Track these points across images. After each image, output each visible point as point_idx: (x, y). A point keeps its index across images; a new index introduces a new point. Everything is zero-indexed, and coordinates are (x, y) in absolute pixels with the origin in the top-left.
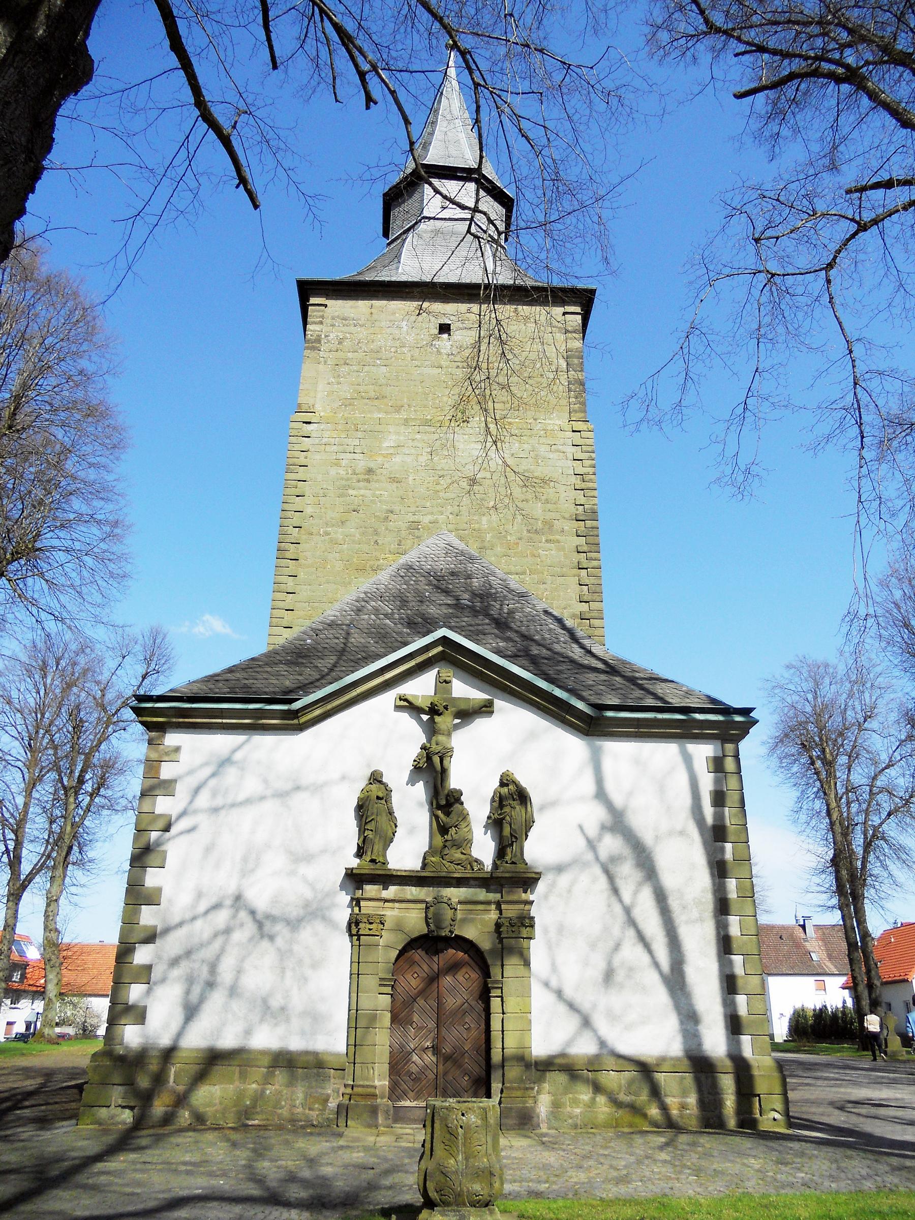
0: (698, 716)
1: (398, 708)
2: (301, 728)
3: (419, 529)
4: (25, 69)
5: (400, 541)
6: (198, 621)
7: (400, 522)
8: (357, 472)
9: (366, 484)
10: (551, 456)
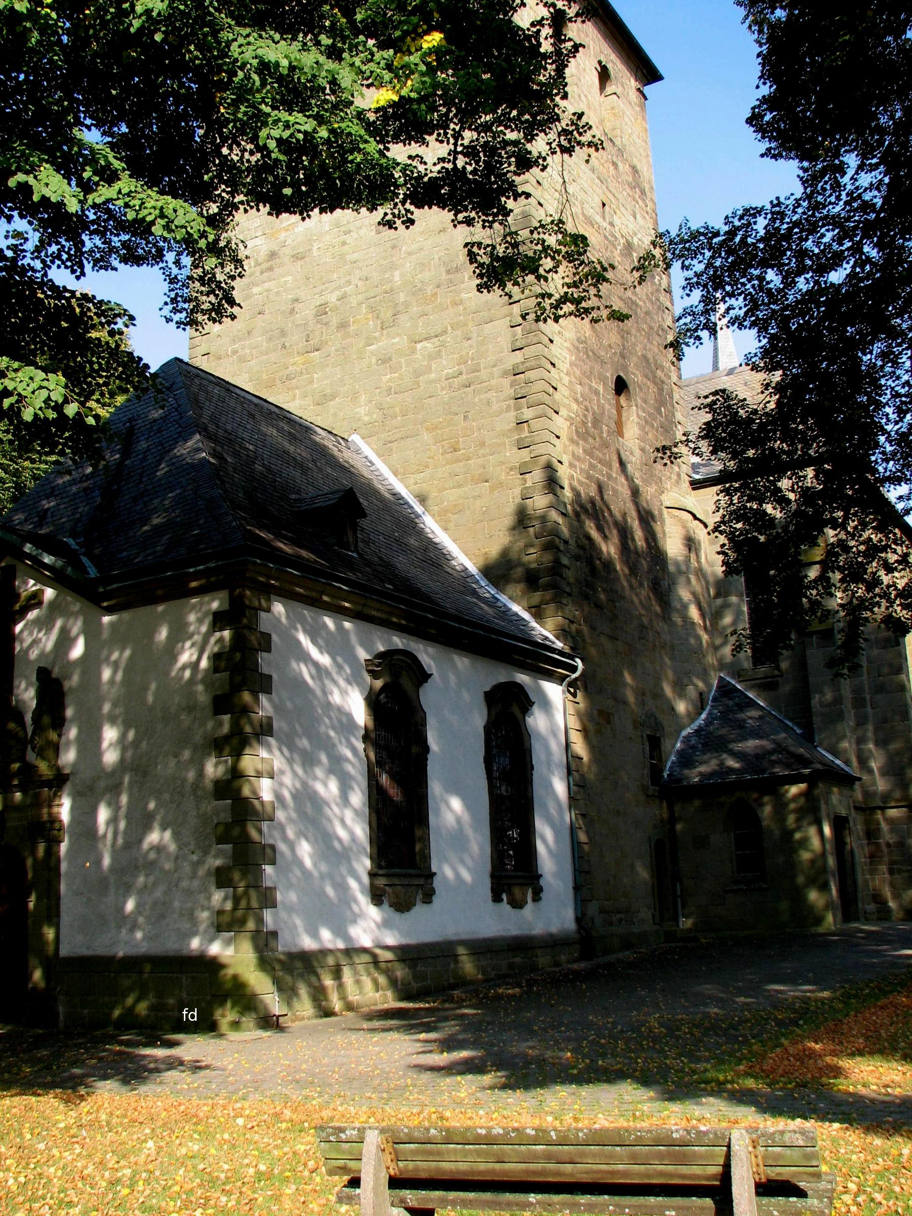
3: (326, 313)
5: (308, 336)
6: (798, 836)
7: (307, 311)
8: (260, 261)
9: (270, 273)
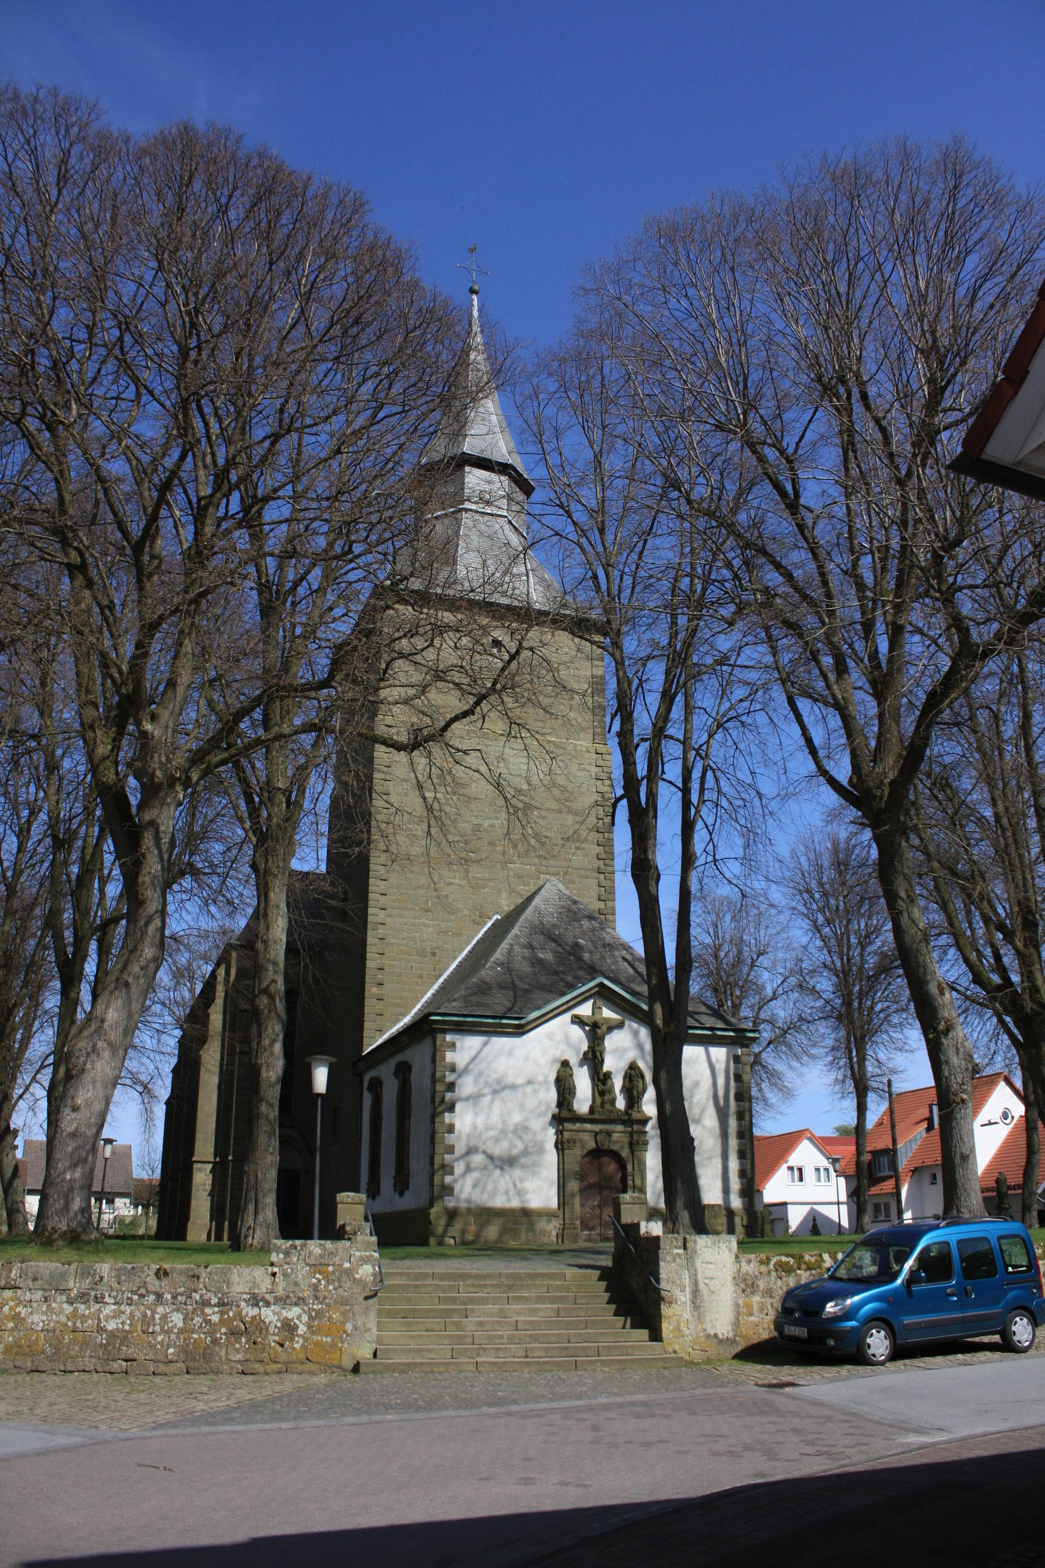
0: (719, 1033)
1: (573, 1022)
2: (523, 1034)
4: (406, 611)
10: (580, 774)
